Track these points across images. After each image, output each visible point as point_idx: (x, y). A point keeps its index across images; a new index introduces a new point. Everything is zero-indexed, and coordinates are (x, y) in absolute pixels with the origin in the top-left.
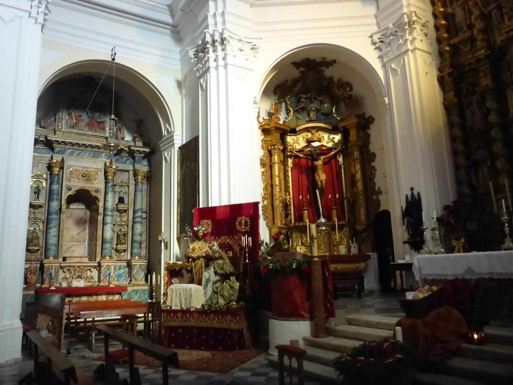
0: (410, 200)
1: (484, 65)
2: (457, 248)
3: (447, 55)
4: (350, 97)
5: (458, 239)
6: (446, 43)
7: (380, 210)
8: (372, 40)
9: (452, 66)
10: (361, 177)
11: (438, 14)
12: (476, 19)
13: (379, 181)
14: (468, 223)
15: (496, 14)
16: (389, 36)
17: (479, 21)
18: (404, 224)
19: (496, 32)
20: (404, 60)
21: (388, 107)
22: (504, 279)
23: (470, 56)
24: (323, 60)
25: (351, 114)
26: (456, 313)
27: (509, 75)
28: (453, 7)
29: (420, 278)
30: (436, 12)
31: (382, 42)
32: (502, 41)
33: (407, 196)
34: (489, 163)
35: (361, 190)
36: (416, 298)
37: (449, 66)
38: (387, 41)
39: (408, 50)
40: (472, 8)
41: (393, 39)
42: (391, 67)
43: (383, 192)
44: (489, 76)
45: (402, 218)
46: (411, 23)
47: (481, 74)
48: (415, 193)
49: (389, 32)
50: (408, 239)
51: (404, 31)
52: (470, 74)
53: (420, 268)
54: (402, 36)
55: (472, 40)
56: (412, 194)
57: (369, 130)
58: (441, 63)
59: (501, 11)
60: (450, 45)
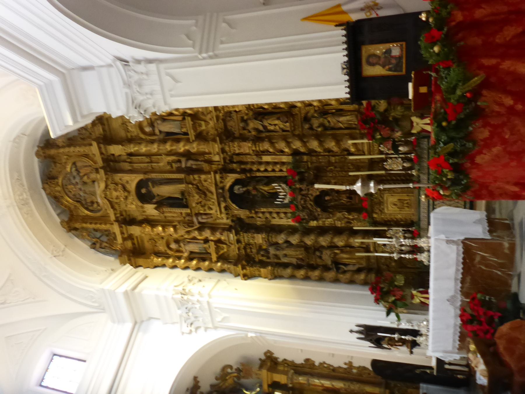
0: (363, 336)
1: (244, 238)
2: (423, 300)
3: (226, 266)
4: (238, 370)
5: (413, 297)
6: (213, 265)
7: (370, 368)
8: (186, 333)
9: (236, 264)
10: (328, 381)
11: (186, 265)
12: (201, 235)
13: (338, 362)
14: (396, 283)
15: (203, 219)
16: (189, 316)
17: (203, 233)
18: (390, 349)
19: (218, 221)
20: (216, 308)
21: (258, 335)
22: (463, 269)
23: (233, 247)
24: (189, 391)
25: (256, 374)
26: (505, 328)
27: (258, 219)
28: (184, 250)
29: (458, 353)
30: (184, 266)
31: (191, 324)
32: (227, 218)
33: (359, 338)
34: (337, 251)
35: (344, 385)
36: (486, 373)
37: (235, 267)
38: (193, 319)
39: (208, 303)
40: (191, 237)
41: (193, 313)
42: (220, 322)
43: (351, 360)
44: (255, 235)
45: (383, 350)
46: (183, 292)
47: (251, 241)
48: (357, 329)
49: (185, 315)
50: (408, 348)
51: (188, 301)
52: (248, 250)
53: (445, 352)
54: (193, 304)
55: (219, 242)
56: (357, 332)
57: (278, 358)
58: (231, 273)
59: (201, 214)
60: (217, 262)
